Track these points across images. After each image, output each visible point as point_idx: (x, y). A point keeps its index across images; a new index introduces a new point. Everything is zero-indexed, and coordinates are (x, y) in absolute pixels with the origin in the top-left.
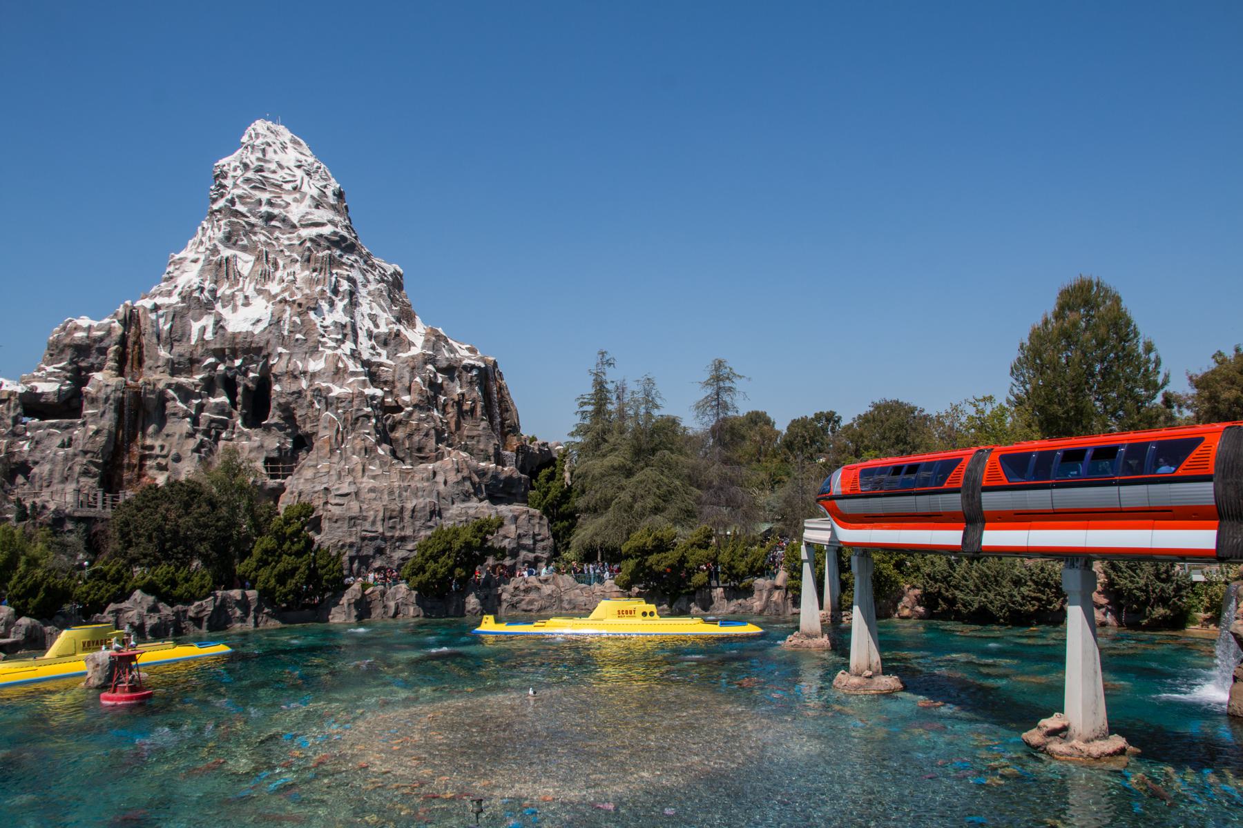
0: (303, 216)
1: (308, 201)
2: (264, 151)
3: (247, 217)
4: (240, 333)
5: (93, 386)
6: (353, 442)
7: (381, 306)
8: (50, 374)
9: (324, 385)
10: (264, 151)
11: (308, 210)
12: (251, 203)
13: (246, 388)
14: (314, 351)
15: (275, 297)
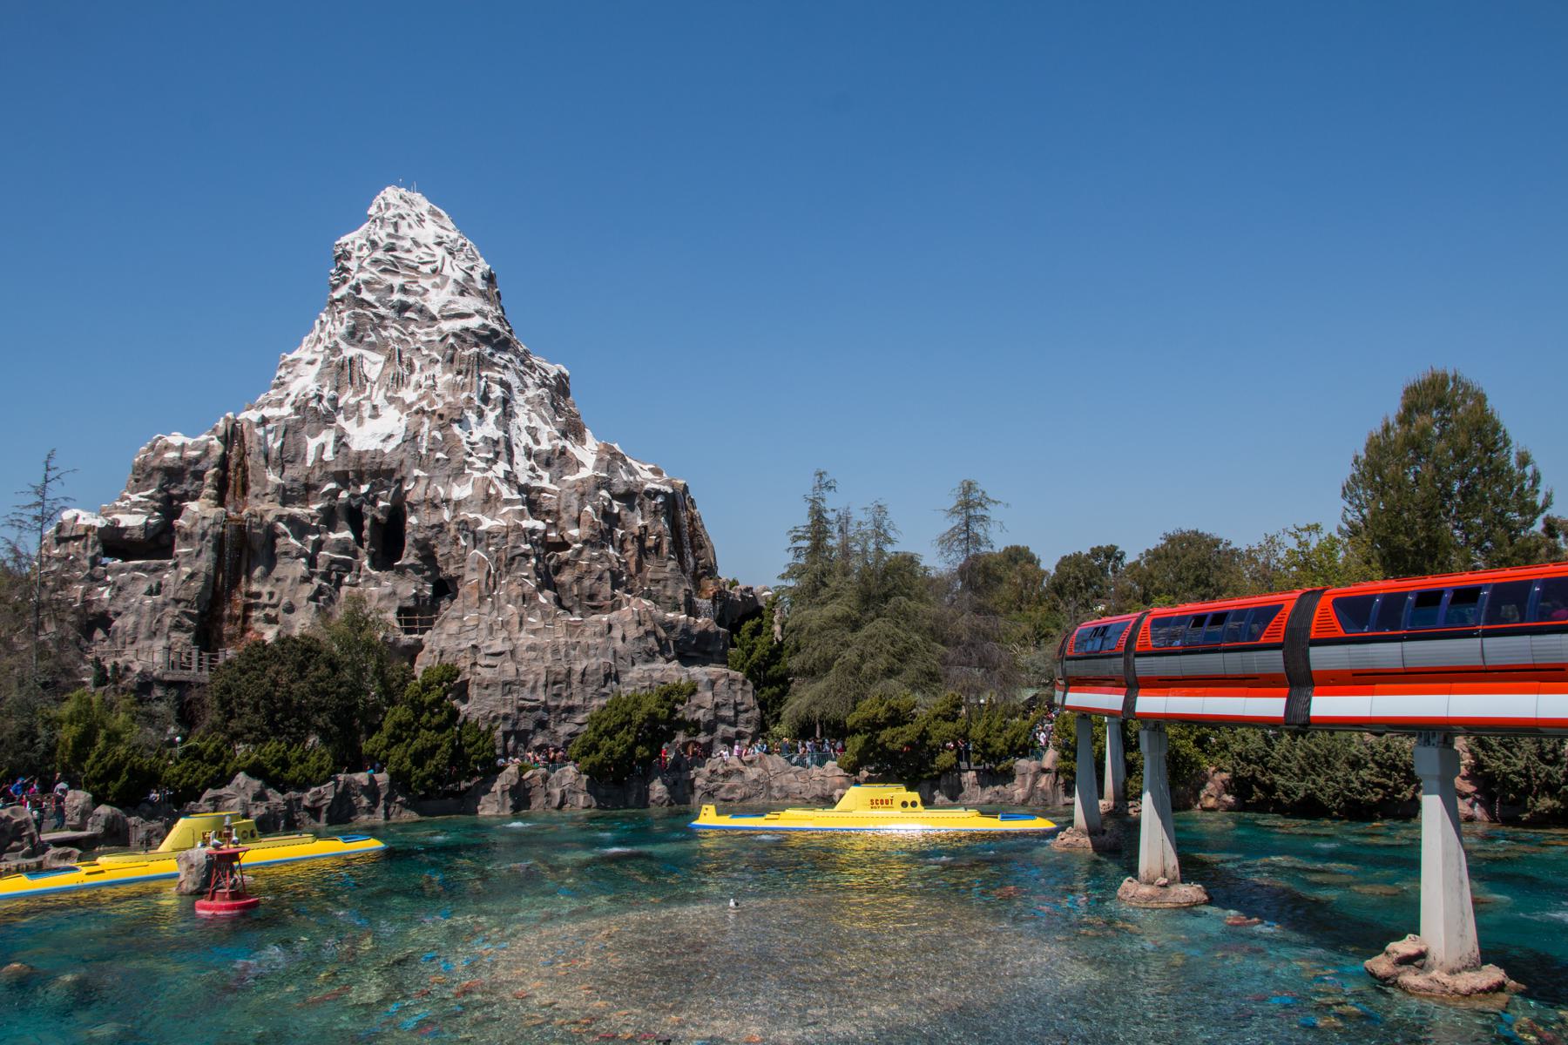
0: (445, 306)
1: (450, 287)
2: (396, 225)
3: (375, 307)
4: (367, 451)
5: (186, 519)
6: (509, 587)
7: (542, 417)
8: (136, 504)
9: (472, 516)
10: (396, 225)
11: (452, 298)
12: (381, 290)
14: (458, 474)
15: (410, 406)
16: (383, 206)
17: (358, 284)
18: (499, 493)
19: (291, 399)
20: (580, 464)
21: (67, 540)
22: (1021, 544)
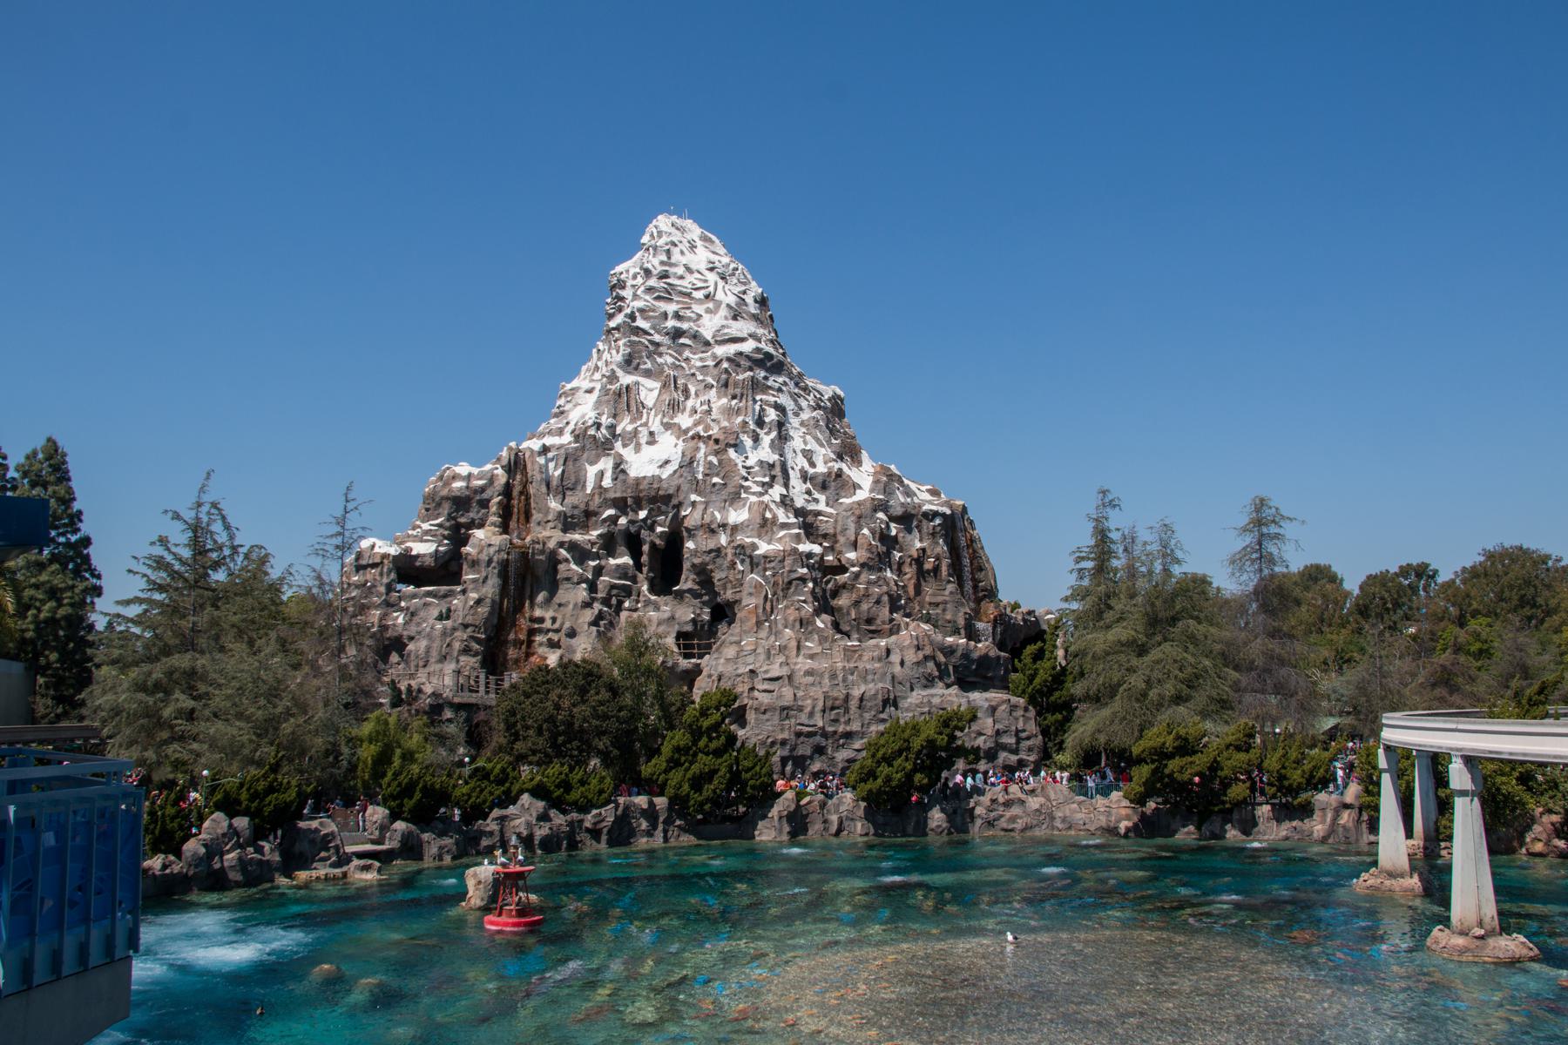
0: (719, 331)
1: (723, 311)
4: (644, 477)
8: (427, 532)
9: (748, 540)
10: (668, 252)
11: (724, 323)
12: (655, 317)
13: (653, 545)
14: (735, 498)
15: (686, 431)
16: (655, 234)
17: (633, 313)
18: (775, 517)
19: (571, 427)
20: (856, 486)
21: (365, 567)
22: (1322, 561)
